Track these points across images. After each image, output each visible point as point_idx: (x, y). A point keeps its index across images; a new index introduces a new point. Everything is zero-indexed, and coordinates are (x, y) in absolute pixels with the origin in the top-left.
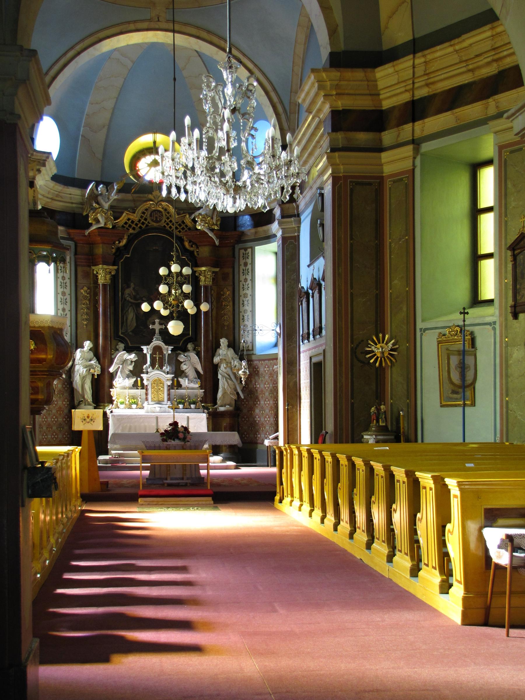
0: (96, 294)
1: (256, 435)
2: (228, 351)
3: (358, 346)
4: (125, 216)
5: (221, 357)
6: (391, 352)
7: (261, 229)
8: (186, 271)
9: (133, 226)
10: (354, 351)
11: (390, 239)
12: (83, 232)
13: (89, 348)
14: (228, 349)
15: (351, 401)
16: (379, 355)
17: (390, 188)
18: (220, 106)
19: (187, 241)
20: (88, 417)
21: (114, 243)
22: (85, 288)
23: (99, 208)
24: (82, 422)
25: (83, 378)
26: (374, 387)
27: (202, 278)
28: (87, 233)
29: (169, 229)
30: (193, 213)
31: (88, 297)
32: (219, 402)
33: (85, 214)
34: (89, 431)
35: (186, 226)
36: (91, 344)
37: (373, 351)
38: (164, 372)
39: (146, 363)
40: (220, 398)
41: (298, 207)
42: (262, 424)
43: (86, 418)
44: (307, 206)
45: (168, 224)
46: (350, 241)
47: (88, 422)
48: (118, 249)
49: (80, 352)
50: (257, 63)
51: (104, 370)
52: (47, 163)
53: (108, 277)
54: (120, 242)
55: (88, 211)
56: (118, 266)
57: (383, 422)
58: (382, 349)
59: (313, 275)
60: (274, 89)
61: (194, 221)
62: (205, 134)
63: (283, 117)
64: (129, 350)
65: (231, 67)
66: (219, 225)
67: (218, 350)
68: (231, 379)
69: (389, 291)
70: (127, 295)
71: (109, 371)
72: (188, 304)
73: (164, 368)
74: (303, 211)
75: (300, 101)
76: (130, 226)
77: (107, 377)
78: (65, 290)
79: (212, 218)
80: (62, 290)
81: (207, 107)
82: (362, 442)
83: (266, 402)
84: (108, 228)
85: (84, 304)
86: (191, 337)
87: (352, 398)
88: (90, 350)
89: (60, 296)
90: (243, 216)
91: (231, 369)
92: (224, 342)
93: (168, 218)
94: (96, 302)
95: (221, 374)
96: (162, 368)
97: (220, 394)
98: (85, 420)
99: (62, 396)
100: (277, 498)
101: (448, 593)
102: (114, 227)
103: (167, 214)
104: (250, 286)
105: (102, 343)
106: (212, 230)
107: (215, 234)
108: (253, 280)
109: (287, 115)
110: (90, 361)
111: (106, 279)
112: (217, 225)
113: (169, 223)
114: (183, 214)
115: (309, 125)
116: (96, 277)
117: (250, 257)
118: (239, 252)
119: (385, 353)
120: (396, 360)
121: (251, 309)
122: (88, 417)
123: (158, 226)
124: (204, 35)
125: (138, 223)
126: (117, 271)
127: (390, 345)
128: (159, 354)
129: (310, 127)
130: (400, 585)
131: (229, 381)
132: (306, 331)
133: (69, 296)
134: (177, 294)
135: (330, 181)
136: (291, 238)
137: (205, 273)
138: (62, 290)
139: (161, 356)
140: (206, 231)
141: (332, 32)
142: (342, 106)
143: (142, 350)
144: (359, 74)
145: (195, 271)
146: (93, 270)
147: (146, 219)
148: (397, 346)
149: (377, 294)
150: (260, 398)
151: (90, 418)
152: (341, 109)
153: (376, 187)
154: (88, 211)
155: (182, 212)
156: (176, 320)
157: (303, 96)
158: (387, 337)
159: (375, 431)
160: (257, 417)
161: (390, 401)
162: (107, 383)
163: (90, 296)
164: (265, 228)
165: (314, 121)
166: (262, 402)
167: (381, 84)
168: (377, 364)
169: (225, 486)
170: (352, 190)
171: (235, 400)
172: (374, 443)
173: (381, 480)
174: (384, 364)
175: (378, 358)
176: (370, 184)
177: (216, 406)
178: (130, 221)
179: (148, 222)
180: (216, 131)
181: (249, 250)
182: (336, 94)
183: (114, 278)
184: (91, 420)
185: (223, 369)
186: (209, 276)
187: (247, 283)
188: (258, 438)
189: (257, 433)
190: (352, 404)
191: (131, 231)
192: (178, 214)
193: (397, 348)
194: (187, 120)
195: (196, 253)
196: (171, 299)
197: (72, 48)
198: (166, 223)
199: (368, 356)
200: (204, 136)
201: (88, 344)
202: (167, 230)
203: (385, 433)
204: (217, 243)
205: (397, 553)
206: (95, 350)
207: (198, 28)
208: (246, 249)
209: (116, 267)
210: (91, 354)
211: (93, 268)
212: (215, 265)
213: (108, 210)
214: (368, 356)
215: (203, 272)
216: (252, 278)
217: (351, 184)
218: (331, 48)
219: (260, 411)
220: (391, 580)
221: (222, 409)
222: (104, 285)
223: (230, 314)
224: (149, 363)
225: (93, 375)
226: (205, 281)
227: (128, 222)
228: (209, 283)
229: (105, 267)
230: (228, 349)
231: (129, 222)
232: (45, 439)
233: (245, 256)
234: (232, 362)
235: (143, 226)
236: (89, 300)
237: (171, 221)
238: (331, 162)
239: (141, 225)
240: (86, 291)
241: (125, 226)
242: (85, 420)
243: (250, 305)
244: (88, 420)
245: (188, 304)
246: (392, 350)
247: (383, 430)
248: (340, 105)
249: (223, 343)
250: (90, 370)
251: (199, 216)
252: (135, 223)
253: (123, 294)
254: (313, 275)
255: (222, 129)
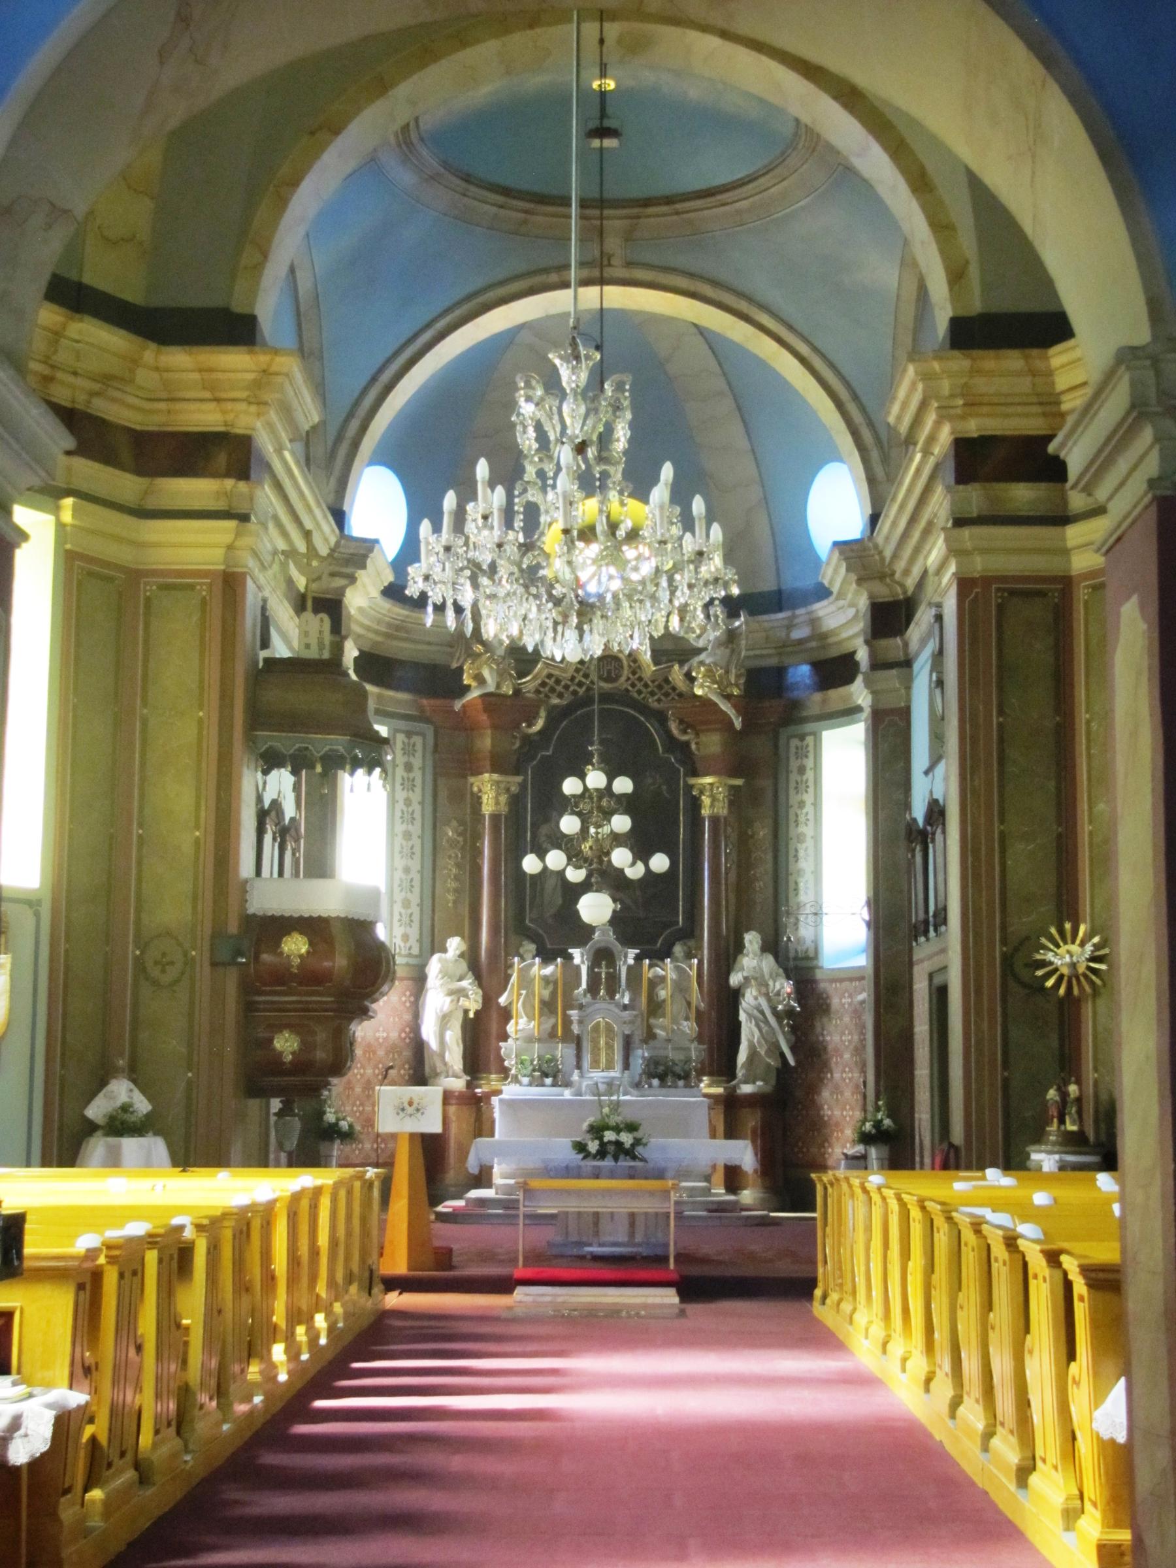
0: (477, 836)
1: (824, 1147)
2: (762, 961)
3: (1016, 949)
4: (541, 669)
5: (745, 974)
6: (1092, 965)
7: (835, 694)
8: (624, 785)
9: (559, 688)
10: (1008, 962)
11: (1087, 712)
12: (446, 702)
13: (458, 952)
14: (762, 955)
15: (1002, 1074)
16: (1065, 971)
17: (1086, 602)
18: (552, 438)
19: (674, 721)
20: (410, 1104)
21: (518, 726)
22: (454, 823)
23: (486, 652)
24: (398, 1114)
25: (444, 1020)
26: (1055, 1043)
27: (706, 800)
28: (458, 705)
29: (635, 695)
30: (688, 660)
31: (458, 842)
32: (740, 1073)
33: (454, 665)
34: (412, 1136)
35: (674, 689)
36: (463, 943)
37: (1051, 963)
38: (617, 1005)
39: (579, 985)
40: (743, 1065)
41: (906, 645)
42: (837, 1124)
43: (406, 1105)
44: (923, 642)
45: (633, 685)
46: (997, 718)
47: (411, 1115)
48: (527, 739)
49: (440, 960)
50: (817, 344)
51: (489, 1000)
52: (369, 561)
53: (503, 799)
54: (530, 725)
55: (461, 660)
56: (526, 774)
57: (1073, 1123)
58: (1071, 956)
59: (931, 792)
60: (855, 397)
61: (691, 679)
62: (518, 496)
63: (875, 455)
64: (547, 956)
65: (577, 358)
66: (742, 687)
67: (739, 957)
68: (766, 1021)
69: (1087, 828)
70: (543, 839)
71: (498, 1004)
72: (621, 857)
73: (618, 996)
74: (917, 655)
75: (891, 419)
76: (553, 690)
77: (494, 1015)
78: (410, 827)
79: (727, 672)
80: (404, 827)
81: (528, 440)
82: (1027, 1169)
83: (362, 1071)
84: (505, 696)
85: (450, 857)
86: (681, 929)
87: (1006, 1064)
88: (462, 955)
89: (399, 840)
90: (797, 665)
91: (769, 1000)
92: (752, 940)
93: (634, 673)
94: (478, 853)
95: (745, 1011)
96: (612, 997)
97: (742, 1056)
98: (403, 1110)
99: (399, 1055)
100: (818, 1293)
101: (1074, 1530)
102: (517, 692)
103: (632, 664)
104: (811, 816)
105: (487, 943)
106: (728, 697)
107: (735, 706)
108: (817, 804)
109: (883, 452)
110: (460, 979)
111: (497, 803)
112: (737, 685)
113: (636, 682)
114: (666, 662)
115: (918, 471)
116: (477, 801)
117: (811, 755)
118: (788, 743)
119: (1078, 965)
120: (1102, 980)
121: (812, 868)
122: (410, 1104)
123: (614, 688)
124: (708, 291)
125: (569, 683)
126: (523, 786)
127: (1089, 948)
128: (607, 967)
129: (921, 475)
130: (1001, 1506)
131: (762, 1025)
132: (921, 916)
133: (419, 841)
134: (600, 836)
135: (953, 592)
136: (893, 711)
137: (712, 790)
138: (404, 827)
139: (611, 970)
140: (715, 698)
141: (956, 277)
142: (978, 430)
143: (570, 957)
144: (1013, 359)
145: (692, 787)
146: (472, 785)
147: (586, 676)
148: (1106, 951)
149: (1059, 836)
150: (833, 1065)
151: (415, 1105)
152: (975, 435)
153: (1056, 600)
154: (461, 660)
155: (664, 659)
156: (597, 891)
157: (895, 409)
158: (1082, 929)
159: (1054, 1144)
160: (826, 1107)
161: (1090, 1075)
162: (494, 1028)
163: (465, 841)
164: (842, 690)
165: (927, 463)
166: (837, 1075)
167: (1062, 382)
168: (1062, 991)
169: (720, 1263)
170: (1000, 608)
171: (777, 1069)
172: (1057, 1170)
173: (971, 1254)
174: (1076, 991)
175: (1061, 977)
176: (1041, 594)
177: (734, 1083)
178: (553, 679)
179: (592, 682)
180: (544, 489)
181: (810, 740)
182: (965, 405)
183: (516, 801)
184: (418, 1110)
185: (750, 999)
186: (721, 797)
187: (804, 811)
188: (827, 1156)
189: (826, 1145)
190: (1006, 1083)
191: (555, 701)
192: (656, 664)
193: (1106, 955)
194: (482, 469)
195: (693, 747)
196: (586, 847)
197: (428, 326)
198: (630, 682)
199: (1039, 973)
200: (516, 500)
201: (455, 945)
202: (632, 698)
203: (1077, 1149)
204: (738, 724)
205: (999, 1429)
206: (471, 958)
207: (691, 275)
208: (802, 738)
209: (519, 779)
210: (463, 966)
211: (472, 779)
212: (734, 771)
213: (504, 658)
214: (1039, 973)
215: (708, 787)
216: (815, 799)
217: (999, 594)
218: (954, 308)
219: (832, 1094)
220: (986, 1493)
221: (747, 1089)
222: (495, 818)
223: (768, 879)
224: (584, 985)
225: (466, 1012)
226: (712, 805)
227: (547, 681)
228: (722, 810)
229: (496, 776)
230: (762, 955)
231: (551, 682)
232: (357, 1152)
233: (802, 753)
234: (771, 983)
235: (579, 690)
236: (463, 849)
237: (640, 679)
238: (954, 551)
239: (576, 688)
240: (455, 831)
241: (542, 689)
242: (403, 1110)
243: (811, 859)
244: (410, 1110)
245: (621, 857)
246: (1093, 959)
247: (1075, 1142)
248: (973, 428)
249: (751, 942)
250: (458, 1000)
251: (699, 667)
252: (563, 683)
253: (534, 836)
254: (931, 792)
255: (554, 487)
